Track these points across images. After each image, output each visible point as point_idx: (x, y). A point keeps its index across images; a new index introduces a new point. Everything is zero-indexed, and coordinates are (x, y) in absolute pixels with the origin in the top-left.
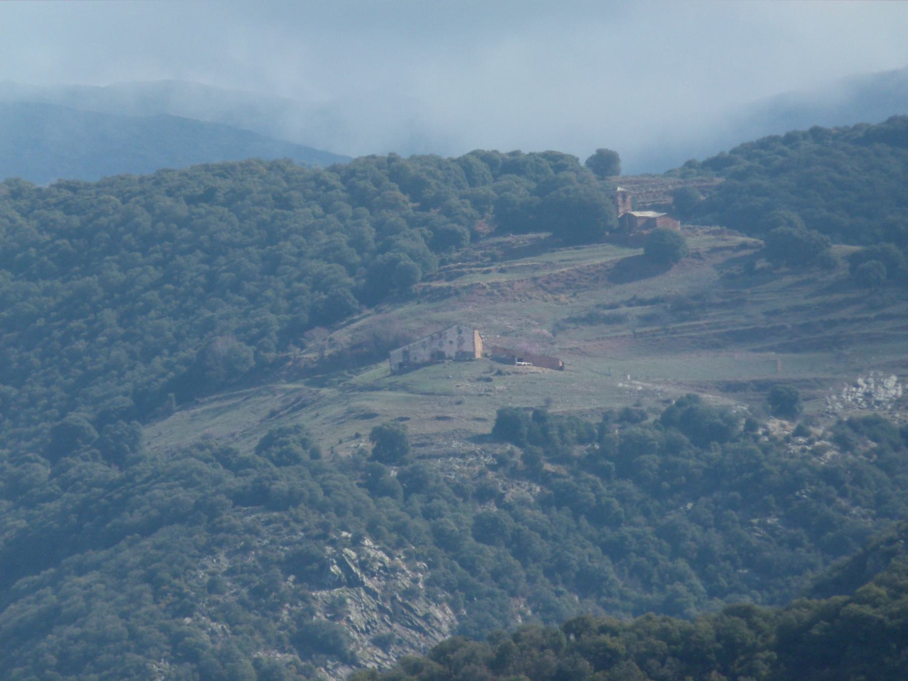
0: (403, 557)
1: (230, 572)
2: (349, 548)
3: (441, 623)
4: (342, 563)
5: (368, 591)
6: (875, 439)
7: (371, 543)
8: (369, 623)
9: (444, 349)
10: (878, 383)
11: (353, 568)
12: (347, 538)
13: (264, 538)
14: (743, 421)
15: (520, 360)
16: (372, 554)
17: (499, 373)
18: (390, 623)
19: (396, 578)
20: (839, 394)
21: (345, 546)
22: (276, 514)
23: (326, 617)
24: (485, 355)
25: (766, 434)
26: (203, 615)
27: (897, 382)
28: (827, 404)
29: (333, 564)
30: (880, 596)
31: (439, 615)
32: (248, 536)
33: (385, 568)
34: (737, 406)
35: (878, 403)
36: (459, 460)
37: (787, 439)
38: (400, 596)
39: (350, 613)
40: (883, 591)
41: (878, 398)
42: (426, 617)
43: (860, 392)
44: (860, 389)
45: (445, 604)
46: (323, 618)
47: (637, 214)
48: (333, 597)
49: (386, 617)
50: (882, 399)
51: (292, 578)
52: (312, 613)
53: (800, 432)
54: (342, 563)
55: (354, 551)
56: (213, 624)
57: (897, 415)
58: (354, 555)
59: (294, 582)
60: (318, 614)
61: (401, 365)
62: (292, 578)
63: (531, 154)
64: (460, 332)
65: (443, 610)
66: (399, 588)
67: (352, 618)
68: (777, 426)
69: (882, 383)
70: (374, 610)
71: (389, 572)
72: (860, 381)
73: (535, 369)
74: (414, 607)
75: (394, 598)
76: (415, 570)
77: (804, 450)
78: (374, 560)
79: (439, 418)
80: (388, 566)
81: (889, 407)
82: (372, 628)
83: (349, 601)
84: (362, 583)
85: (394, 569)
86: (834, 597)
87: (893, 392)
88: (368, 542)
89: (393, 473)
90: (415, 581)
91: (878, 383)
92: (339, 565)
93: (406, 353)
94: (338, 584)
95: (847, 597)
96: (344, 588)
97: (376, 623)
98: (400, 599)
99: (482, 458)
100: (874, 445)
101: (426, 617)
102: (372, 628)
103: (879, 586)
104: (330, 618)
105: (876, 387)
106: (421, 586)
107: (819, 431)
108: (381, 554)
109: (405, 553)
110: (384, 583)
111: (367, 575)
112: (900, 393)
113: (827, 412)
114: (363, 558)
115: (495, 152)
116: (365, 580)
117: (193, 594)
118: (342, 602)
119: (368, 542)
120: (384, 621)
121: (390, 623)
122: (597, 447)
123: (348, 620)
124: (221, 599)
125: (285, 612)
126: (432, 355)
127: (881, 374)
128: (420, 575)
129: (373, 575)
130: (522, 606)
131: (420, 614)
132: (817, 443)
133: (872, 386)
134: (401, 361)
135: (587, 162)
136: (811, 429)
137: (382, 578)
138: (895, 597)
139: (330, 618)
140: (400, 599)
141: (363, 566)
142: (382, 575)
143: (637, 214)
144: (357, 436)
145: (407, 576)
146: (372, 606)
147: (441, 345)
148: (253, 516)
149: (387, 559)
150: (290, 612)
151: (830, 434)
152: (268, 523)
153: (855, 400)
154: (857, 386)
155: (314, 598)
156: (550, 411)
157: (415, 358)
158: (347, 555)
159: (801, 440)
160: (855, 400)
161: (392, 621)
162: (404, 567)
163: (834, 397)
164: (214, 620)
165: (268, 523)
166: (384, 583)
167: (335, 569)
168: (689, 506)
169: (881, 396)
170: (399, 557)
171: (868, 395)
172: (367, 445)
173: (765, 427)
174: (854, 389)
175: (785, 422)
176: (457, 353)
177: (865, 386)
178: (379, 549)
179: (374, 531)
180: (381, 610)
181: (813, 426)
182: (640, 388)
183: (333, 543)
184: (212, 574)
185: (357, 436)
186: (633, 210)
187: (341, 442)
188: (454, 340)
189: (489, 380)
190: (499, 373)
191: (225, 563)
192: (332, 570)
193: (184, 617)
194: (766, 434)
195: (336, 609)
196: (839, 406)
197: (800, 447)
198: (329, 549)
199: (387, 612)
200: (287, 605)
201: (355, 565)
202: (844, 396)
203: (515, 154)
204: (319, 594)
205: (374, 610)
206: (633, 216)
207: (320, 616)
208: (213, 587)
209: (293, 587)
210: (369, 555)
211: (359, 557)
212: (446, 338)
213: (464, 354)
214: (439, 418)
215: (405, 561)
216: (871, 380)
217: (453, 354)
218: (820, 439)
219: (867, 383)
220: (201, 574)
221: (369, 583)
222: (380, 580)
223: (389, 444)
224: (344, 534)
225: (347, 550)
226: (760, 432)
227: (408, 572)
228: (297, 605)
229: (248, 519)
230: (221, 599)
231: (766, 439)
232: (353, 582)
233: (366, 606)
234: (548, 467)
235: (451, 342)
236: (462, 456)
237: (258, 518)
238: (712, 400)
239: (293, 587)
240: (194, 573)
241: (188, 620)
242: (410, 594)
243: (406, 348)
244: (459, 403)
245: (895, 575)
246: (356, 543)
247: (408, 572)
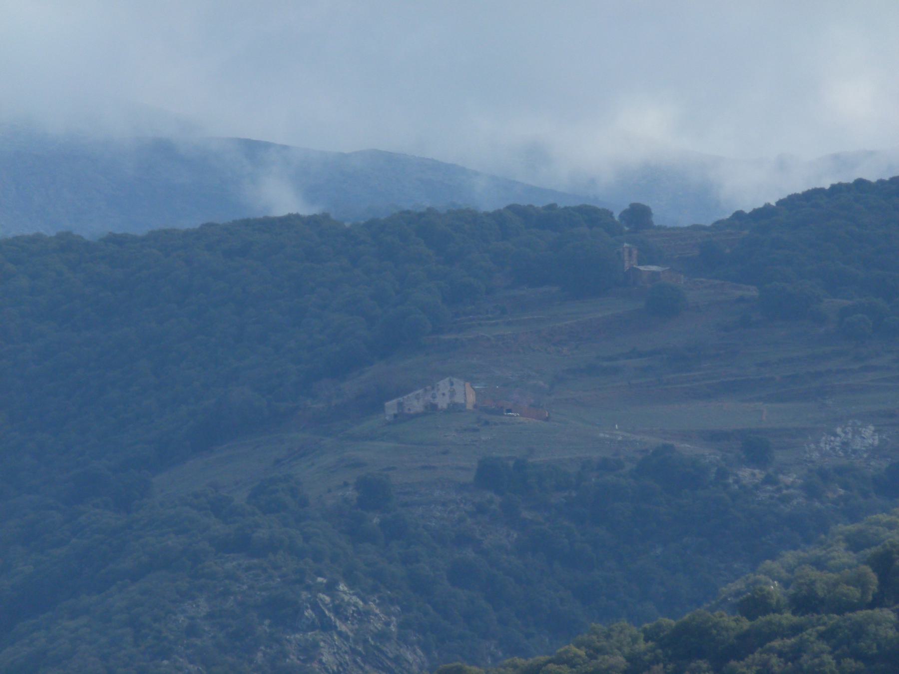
0: (377, 601)
1: (210, 616)
2: (324, 593)
3: (411, 665)
4: (315, 607)
5: (340, 634)
6: (845, 487)
7: (346, 589)
8: (341, 664)
9: (437, 401)
10: (856, 432)
11: (327, 612)
12: (321, 583)
13: (243, 584)
14: (714, 470)
15: (509, 411)
16: (346, 598)
17: (487, 423)
18: (362, 665)
19: (370, 622)
20: (817, 442)
21: (319, 591)
22: (256, 561)
23: (299, 659)
24: (475, 406)
25: (737, 482)
26: (181, 657)
27: (875, 431)
28: (805, 452)
29: (307, 608)
30: (579, 657)
31: (410, 657)
32: (227, 582)
33: (359, 613)
34: (710, 455)
35: (855, 452)
36: (440, 508)
37: (756, 487)
38: (373, 639)
39: (322, 655)
40: (582, 652)
41: (855, 447)
42: (397, 659)
43: (837, 442)
44: (838, 439)
45: (416, 647)
46: (296, 660)
47: (642, 268)
48: (307, 640)
49: (359, 659)
50: (858, 448)
51: (267, 622)
52: (286, 656)
53: (769, 480)
54: (315, 607)
55: (328, 595)
56: (191, 666)
57: (872, 463)
58: (328, 599)
59: (270, 626)
60: (292, 657)
61: (395, 416)
62: (267, 622)
63: (566, 208)
64: (452, 384)
65: (414, 651)
66: (371, 631)
67: (324, 659)
68: (747, 475)
69: (860, 433)
70: (346, 652)
71: (363, 616)
72: (839, 430)
73: (522, 419)
74: (384, 649)
75: (366, 641)
76: (388, 614)
77: (772, 498)
78: (349, 604)
79: (424, 468)
80: (361, 609)
81: (865, 456)
82: (345, 669)
83: (322, 644)
84: (336, 627)
85: (368, 613)
86: (537, 657)
87: (870, 441)
88: (342, 587)
89: (376, 520)
90: (387, 624)
91: (856, 432)
92: (313, 610)
93: (400, 405)
94: (312, 627)
95: (548, 657)
96: (317, 631)
97: (348, 665)
98: (372, 643)
99: (462, 506)
100: (842, 492)
101: (397, 659)
102: (345, 669)
103: (579, 648)
104: (304, 661)
105: (853, 436)
106: (393, 628)
107: (789, 480)
108: (355, 599)
109: (379, 598)
110: (357, 626)
111: (340, 619)
112: (876, 442)
113: (805, 461)
114: (337, 602)
115: (531, 206)
116: (338, 623)
117: (172, 637)
118: (315, 646)
119: (342, 587)
120: (355, 662)
121: (362, 665)
122: (574, 494)
123: (320, 662)
124: (198, 642)
125: (260, 654)
126: (426, 407)
127: (859, 424)
128: (394, 618)
129: (347, 619)
130: (492, 648)
131: (390, 655)
132: (785, 492)
133: (850, 436)
134: (396, 412)
135: (620, 216)
136: (781, 477)
137: (355, 621)
138: (592, 657)
139: (304, 661)
140: (372, 643)
141: (338, 610)
142: (355, 618)
143: (642, 268)
144: (346, 484)
145: (380, 619)
146: (345, 648)
147: (434, 397)
148: (234, 563)
149: (361, 603)
150: (265, 654)
151: (800, 482)
152: (248, 569)
153: (833, 449)
154: (836, 435)
155: (287, 640)
156: (530, 460)
157: (409, 409)
158: (321, 600)
159: (769, 488)
160: (833, 449)
161: (364, 662)
162: (377, 611)
163: (812, 446)
164: (191, 662)
165: (248, 569)
166: (357, 626)
167: (309, 613)
168: (659, 551)
169: (857, 445)
170: (374, 601)
171: (845, 444)
172: (351, 493)
173: (737, 475)
174: (832, 438)
175: (757, 471)
176: (449, 405)
177: (843, 435)
178: (354, 594)
179: (350, 578)
180: (354, 651)
181: (784, 474)
182: (620, 438)
183: (308, 588)
184: (192, 618)
185: (346, 484)
186: (639, 265)
187: (329, 491)
188: (446, 392)
189: (476, 430)
190: (487, 423)
191: (204, 607)
192: (306, 614)
193: (162, 660)
194: (737, 482)
195: (309, 651)
196: (816, 455)
197: (768, 495)
198: (305, 595)
199: (359, 654)
200: (263, 648)
201: (329, 610)
202: (822, 445)
203: (552, 207)
204: (292, 637)
205: (346, 652)
206: (639, 270)
207: (293, 659)
208: (192, 631)
209: (268, 630)
210: (343, 600)
211: (333, 601)
212: (438, 390)
213: (455, 405)
214: (424, 468)
215: (378, 605)
216: (849, 429)
217: (445, 406)
218: (787, 487)
219: (846, 433)
220: (181, 618)
221: (343, 628)
222: (353, 624)
223: (373, 492)
224: (320, 579)
225: (321, 595)
226: (731, 481)
227: (381, 615)
228: (271, 648)
229: (229, 566)
230: (198, 642)
231: (736, 487)
232: (327, 627)
233: (339, 648)
234: (526, 514)
235: (444, 394)
236: (444, 504)
237: (240, 565)
238: (686, 448)
239: (268, 630)
240: (174, 617)
241: (165, 662)
242: (382, 636)
243: (400, 399)
244: (445, 453)
245: (594, 637)
246: (330, 588)
247: (381, 615)
